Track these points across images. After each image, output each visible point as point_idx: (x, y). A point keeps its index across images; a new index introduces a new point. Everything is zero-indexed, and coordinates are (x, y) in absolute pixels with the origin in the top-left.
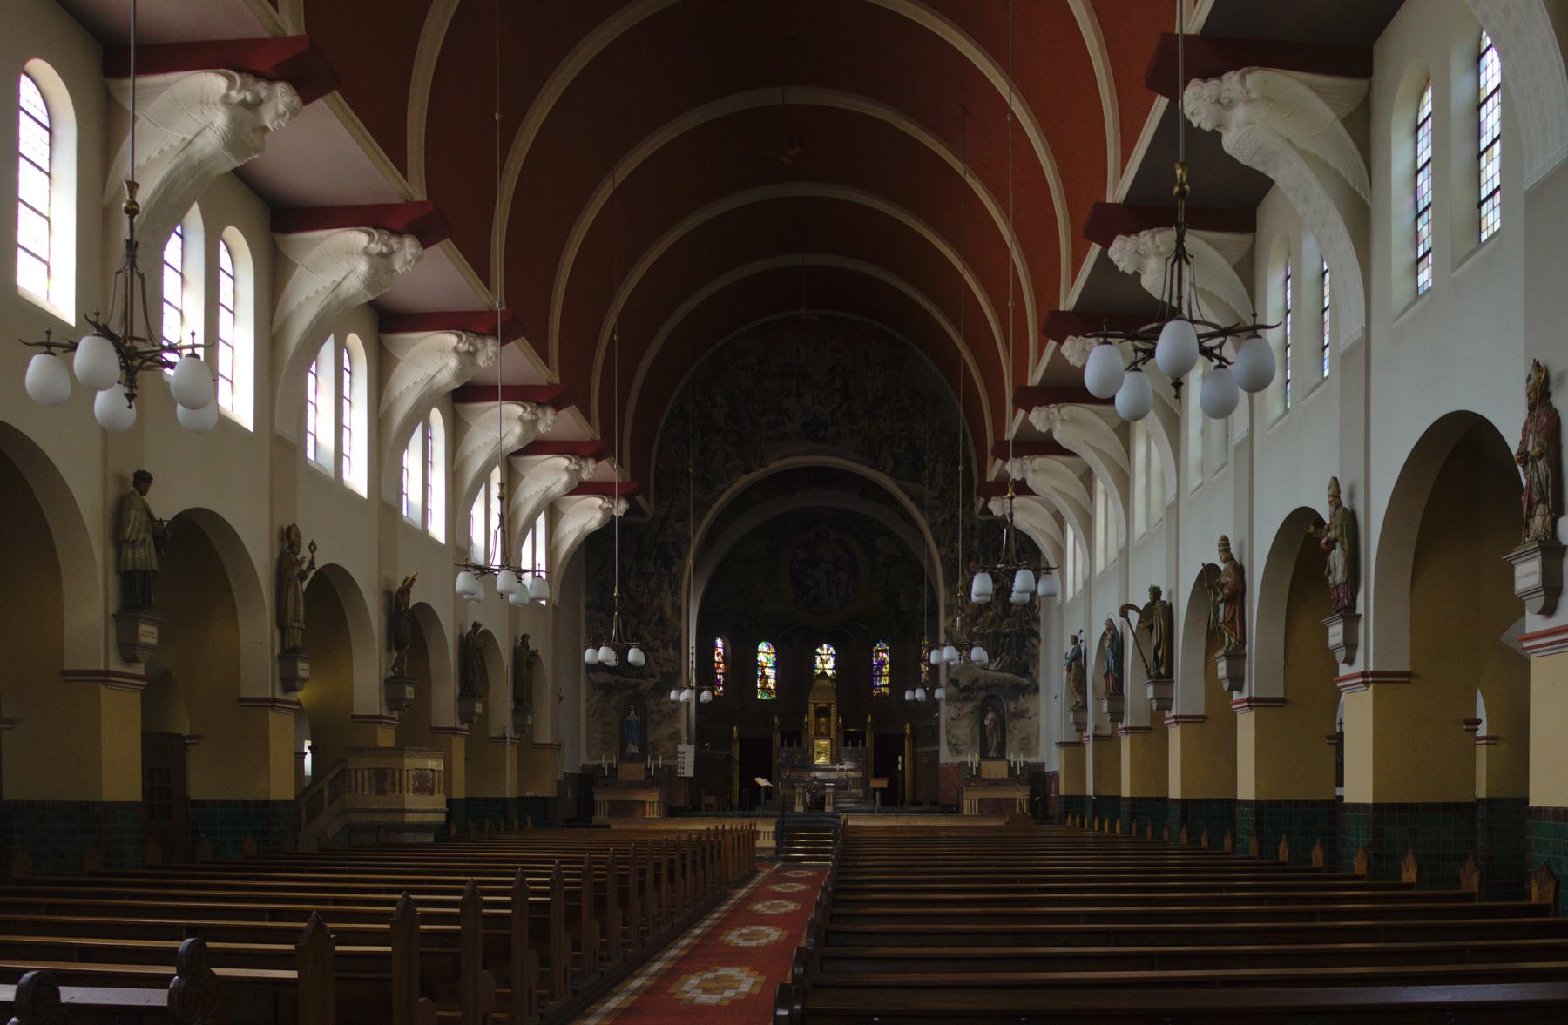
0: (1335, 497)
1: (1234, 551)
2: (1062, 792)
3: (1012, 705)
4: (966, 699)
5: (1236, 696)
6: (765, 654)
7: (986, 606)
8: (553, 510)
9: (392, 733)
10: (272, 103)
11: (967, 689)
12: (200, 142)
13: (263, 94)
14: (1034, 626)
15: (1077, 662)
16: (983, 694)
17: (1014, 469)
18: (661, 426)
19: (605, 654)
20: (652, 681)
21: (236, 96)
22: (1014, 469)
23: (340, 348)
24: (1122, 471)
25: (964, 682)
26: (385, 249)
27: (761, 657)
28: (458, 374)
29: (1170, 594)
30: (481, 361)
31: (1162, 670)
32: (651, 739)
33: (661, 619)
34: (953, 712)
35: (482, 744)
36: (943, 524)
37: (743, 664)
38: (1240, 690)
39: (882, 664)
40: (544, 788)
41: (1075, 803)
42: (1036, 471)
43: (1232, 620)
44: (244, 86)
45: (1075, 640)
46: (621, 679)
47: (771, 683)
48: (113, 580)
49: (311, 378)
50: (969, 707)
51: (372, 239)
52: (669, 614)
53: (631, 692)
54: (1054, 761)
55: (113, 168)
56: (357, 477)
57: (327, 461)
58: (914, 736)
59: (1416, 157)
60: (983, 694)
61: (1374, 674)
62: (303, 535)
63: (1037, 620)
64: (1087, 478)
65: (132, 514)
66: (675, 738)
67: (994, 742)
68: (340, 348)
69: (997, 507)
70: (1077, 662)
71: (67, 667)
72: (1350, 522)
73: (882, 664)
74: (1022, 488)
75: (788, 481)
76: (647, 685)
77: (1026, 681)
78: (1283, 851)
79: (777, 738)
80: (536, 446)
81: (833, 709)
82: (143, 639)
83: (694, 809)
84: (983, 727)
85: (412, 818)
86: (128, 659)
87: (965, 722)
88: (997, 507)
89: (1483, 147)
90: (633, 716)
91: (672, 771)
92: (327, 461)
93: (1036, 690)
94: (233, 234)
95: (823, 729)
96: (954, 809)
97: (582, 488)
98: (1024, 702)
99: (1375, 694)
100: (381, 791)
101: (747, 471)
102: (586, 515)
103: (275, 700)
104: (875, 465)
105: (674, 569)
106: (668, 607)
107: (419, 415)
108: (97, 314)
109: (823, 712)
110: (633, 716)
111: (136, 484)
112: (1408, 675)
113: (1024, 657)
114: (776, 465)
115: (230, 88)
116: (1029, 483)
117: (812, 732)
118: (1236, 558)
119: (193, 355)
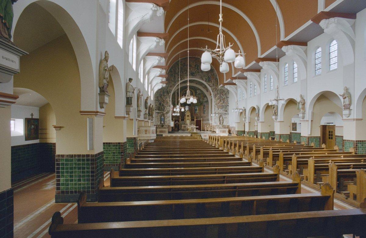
7: (198, 100)
10: (160, 11)
12: (145, 17)
14: (228, 104)
17: (234, 81)
20: (166, 112)
21: (153, 9)
24: (260, 83)
26: (159, 41)
28: (158, 63)
30: (162, 61)
32: (165, 121)
36: (214, 89)
44: (155, 7)
46: (160, 112)
48: (126, 98)
52: (168, 102)
53: (162, 113)
55: (127, 20)
58: (203, 120)
63: (229, 104)
67: (221, 122)
71: (82, 110)
73: (197, 109)
77: (226, 113)
78: (251, 136)
81: (190, 115)
90: (162, 117)
93: (228, 114)
95: (188, 118)
98: (226, 116)
103: (97, 112)
105: (169, 95)
106: (168, 100)
109: (188, 116)
110: (162, 117)
111: (129, 81)
112: (362, 119)
113: (227, 109)
115: (153, 7)
117: (186, 119)
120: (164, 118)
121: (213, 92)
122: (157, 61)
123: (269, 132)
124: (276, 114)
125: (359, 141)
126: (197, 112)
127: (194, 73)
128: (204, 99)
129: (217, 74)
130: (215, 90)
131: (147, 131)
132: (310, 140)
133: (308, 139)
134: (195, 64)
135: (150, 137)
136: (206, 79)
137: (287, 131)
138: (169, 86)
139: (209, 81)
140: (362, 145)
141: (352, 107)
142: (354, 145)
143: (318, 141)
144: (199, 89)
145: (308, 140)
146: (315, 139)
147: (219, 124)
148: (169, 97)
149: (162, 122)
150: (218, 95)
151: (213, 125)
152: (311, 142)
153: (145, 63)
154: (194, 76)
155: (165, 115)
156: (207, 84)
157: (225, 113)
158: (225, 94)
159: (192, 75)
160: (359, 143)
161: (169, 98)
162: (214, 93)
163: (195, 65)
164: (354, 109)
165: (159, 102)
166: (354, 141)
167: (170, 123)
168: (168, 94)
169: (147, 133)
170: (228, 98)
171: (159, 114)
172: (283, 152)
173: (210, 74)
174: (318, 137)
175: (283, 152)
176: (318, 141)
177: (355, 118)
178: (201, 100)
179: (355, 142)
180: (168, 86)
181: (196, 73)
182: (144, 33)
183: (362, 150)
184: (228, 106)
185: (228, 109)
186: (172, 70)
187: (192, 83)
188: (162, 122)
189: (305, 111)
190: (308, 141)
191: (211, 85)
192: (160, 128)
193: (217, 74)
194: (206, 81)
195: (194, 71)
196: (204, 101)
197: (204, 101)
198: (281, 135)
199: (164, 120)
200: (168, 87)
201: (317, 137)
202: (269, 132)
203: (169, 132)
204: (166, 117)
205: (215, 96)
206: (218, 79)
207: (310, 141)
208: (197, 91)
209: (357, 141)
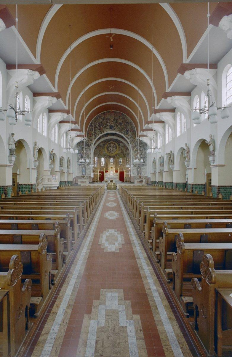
0: (211, 137)
1: (188, 145)
2: (151, 180)
3: (142, 167)
4: (135, 167)
5: (188, 168)
6: (103, 160)
8: (73, 140)
9: (15, 158)
11: (136, 165)
13: (34, 73)
14: (146, 156)
15: (155, 161)
16: (138, 166)
18: (88, 127)
19: (83, 160)
20: (87, 164)
21: (29, 74)
22: (145, 133)
23: (43, 115)
25: (135, 164)
27: (102, 160)
29: (174, 152)
31: (173, 163)
32: (86, 172)
33: (88, 155)
34: (133, 168)
35: (62, 173)
37: (99, 162)
38: (189, 167)
39: (120, 161)
40: (71, 179)
41: (154, 183)
42: (150, 134)
43: (188, 156)
45: (154, 158)
47: (104, 164)
49: (38, 119)
50: (136, 168)
51: (49, 98)
54: (149, 176)
56: (56, 142)
57: (41, 132)
58: (126, 172)
59: (227, 81)
60: (138, 166)
61: (218, 165)
62: (37, 143)
64: (156, 134)
65: (11, 140)
66: (90, 172)
68: (43, 115)
69: (141, 139)
70: (155, 161)
72: (213, 141)
74: (146, 136)
75: (107, 135)
76: (86, 164)
79: (104, 172)
80: (72, 130)
82: (13, 160)
83: (93, 182)
84: (138, 170)
85: (53, 186)
86: (10, 163)
87: (135, 170)
88: (141, 139)
89: (227, 83)
91: (90, 177)
92: (41, 132)
93: (146, 165)
94: (27, 97)
96: (133, 183)
97: (78, 136)
98: (144, 167)
99: (219, 168)
100: (49, 181)
101: (101, 133)
102: (78, 140)
104: (121, 132)
107: (64, 133)
108: (11, 105)
110: (84, 169)
112: (224, 165)
114: (105, 133)
116: (147, 135)
118: (188, 146)
119: (28, 113)
120: (85, 170)
121: (131, 144)
122: (60, 117)
123: (204, 183)
124: (173, 163)
125: (221, 186)
126: (121, 164)
127: (113, 127)
128: (126, 151)
129: (135, 127)
130: (133, 141)
131: (50, 180)
132: (194, 187)
133: (192, 186)
134: (114, 118)
135: (52, 184)
136: (124, 132)
137: (203, 181)
138: (90, 139)
139: (128, 134)
140: (225, 191)
141: (216, 154)
142: (217, 190)
143: (203, 189)
144: (121, 142)
145: (192, 187)
146: (199, 187)
147: (136, 175)
148: (89, 150)
149: (84, 173)
150: (136, 147)
151: (131, 175)
152: (195, 189)
153: (50, 118)
154: (113, 129)
155: (86, 167)
156: (126, 136)
157: (143, 165)
158: (143, 145)
159: (111, 129)
160: (221, 189)
161: (90, 151)
162: (132, 145)
163: (114, 119)
164: (217, 156)
165: (81, 155)
166: (217, 186)
167: (90, 174)
168: (89, 147)
169: (50, 181)
170: (146, 149)
171: (81, 166)
172: (136, 197)
173: (128, 127)
174: (203, 184)
175: (136, 197)
176: (203, 189)
177: (218, 164)
178: (124, 152)
179: (218, 188)
180: (88, 139)
181: (115, 127)
182: (40, 93)
183: (225, 195)
184: (146, 157)
185: (146, 160)
186: (92, 124)
187: (114, 136)
188: (84, 173)
189: (189, 159)
190: (192, 189)
191: (130, 137)
192: (81, 179)
193: (135, 127)
194: (124, 134)
195: (113, 125)
196: (127, 153)
197: (127, 153)
198: (177, 183)
199: (85, 172)
200: (88, 141)
201: (201, 184)
202: (204, 183)
203: (90, 183)
204: (87, 169)
205: (133, 147)
206: (135, 132)
207: (194, 188)
208: (120, 144)
209: (219, 186)
